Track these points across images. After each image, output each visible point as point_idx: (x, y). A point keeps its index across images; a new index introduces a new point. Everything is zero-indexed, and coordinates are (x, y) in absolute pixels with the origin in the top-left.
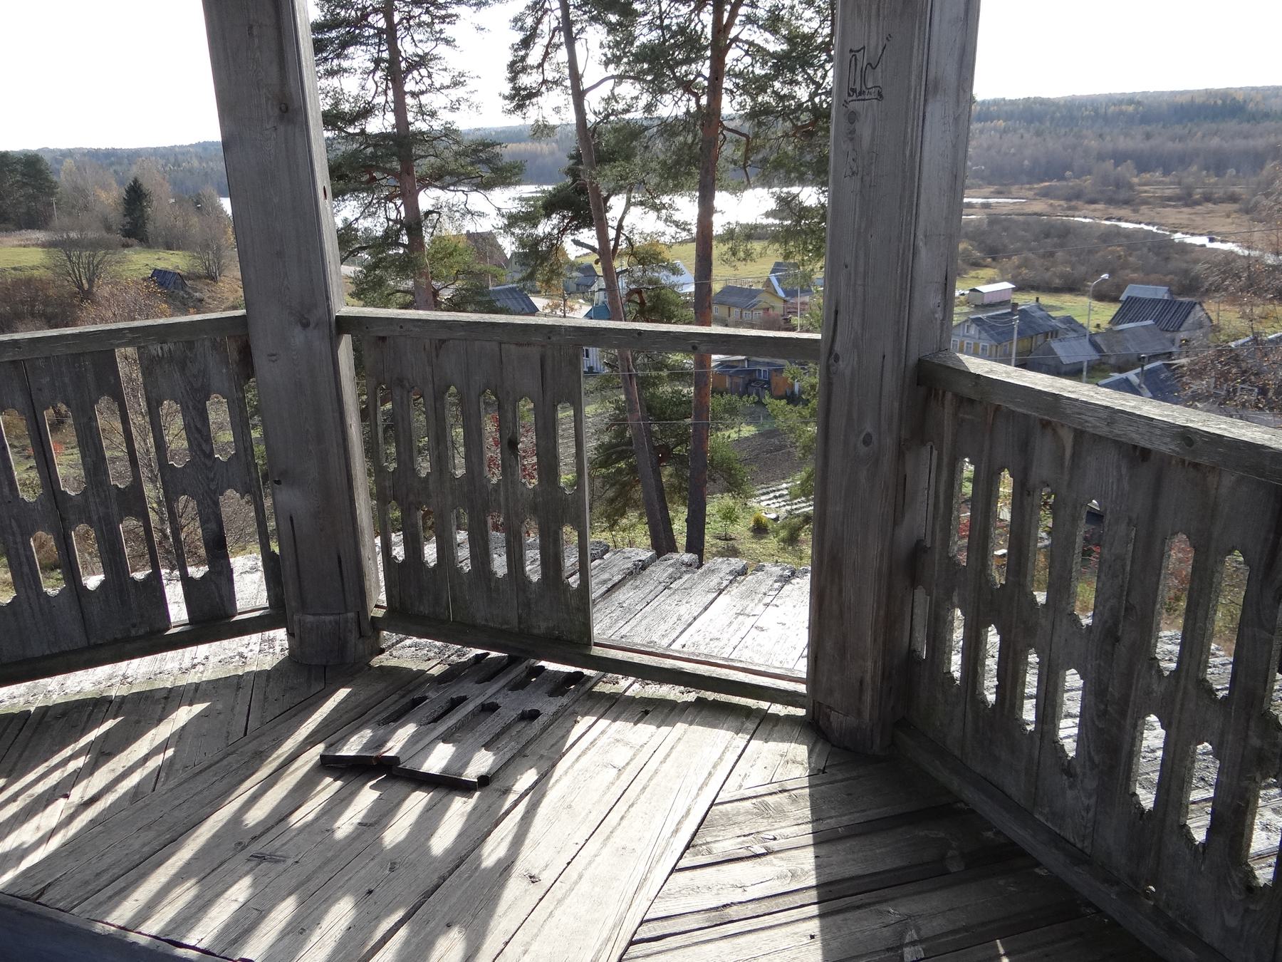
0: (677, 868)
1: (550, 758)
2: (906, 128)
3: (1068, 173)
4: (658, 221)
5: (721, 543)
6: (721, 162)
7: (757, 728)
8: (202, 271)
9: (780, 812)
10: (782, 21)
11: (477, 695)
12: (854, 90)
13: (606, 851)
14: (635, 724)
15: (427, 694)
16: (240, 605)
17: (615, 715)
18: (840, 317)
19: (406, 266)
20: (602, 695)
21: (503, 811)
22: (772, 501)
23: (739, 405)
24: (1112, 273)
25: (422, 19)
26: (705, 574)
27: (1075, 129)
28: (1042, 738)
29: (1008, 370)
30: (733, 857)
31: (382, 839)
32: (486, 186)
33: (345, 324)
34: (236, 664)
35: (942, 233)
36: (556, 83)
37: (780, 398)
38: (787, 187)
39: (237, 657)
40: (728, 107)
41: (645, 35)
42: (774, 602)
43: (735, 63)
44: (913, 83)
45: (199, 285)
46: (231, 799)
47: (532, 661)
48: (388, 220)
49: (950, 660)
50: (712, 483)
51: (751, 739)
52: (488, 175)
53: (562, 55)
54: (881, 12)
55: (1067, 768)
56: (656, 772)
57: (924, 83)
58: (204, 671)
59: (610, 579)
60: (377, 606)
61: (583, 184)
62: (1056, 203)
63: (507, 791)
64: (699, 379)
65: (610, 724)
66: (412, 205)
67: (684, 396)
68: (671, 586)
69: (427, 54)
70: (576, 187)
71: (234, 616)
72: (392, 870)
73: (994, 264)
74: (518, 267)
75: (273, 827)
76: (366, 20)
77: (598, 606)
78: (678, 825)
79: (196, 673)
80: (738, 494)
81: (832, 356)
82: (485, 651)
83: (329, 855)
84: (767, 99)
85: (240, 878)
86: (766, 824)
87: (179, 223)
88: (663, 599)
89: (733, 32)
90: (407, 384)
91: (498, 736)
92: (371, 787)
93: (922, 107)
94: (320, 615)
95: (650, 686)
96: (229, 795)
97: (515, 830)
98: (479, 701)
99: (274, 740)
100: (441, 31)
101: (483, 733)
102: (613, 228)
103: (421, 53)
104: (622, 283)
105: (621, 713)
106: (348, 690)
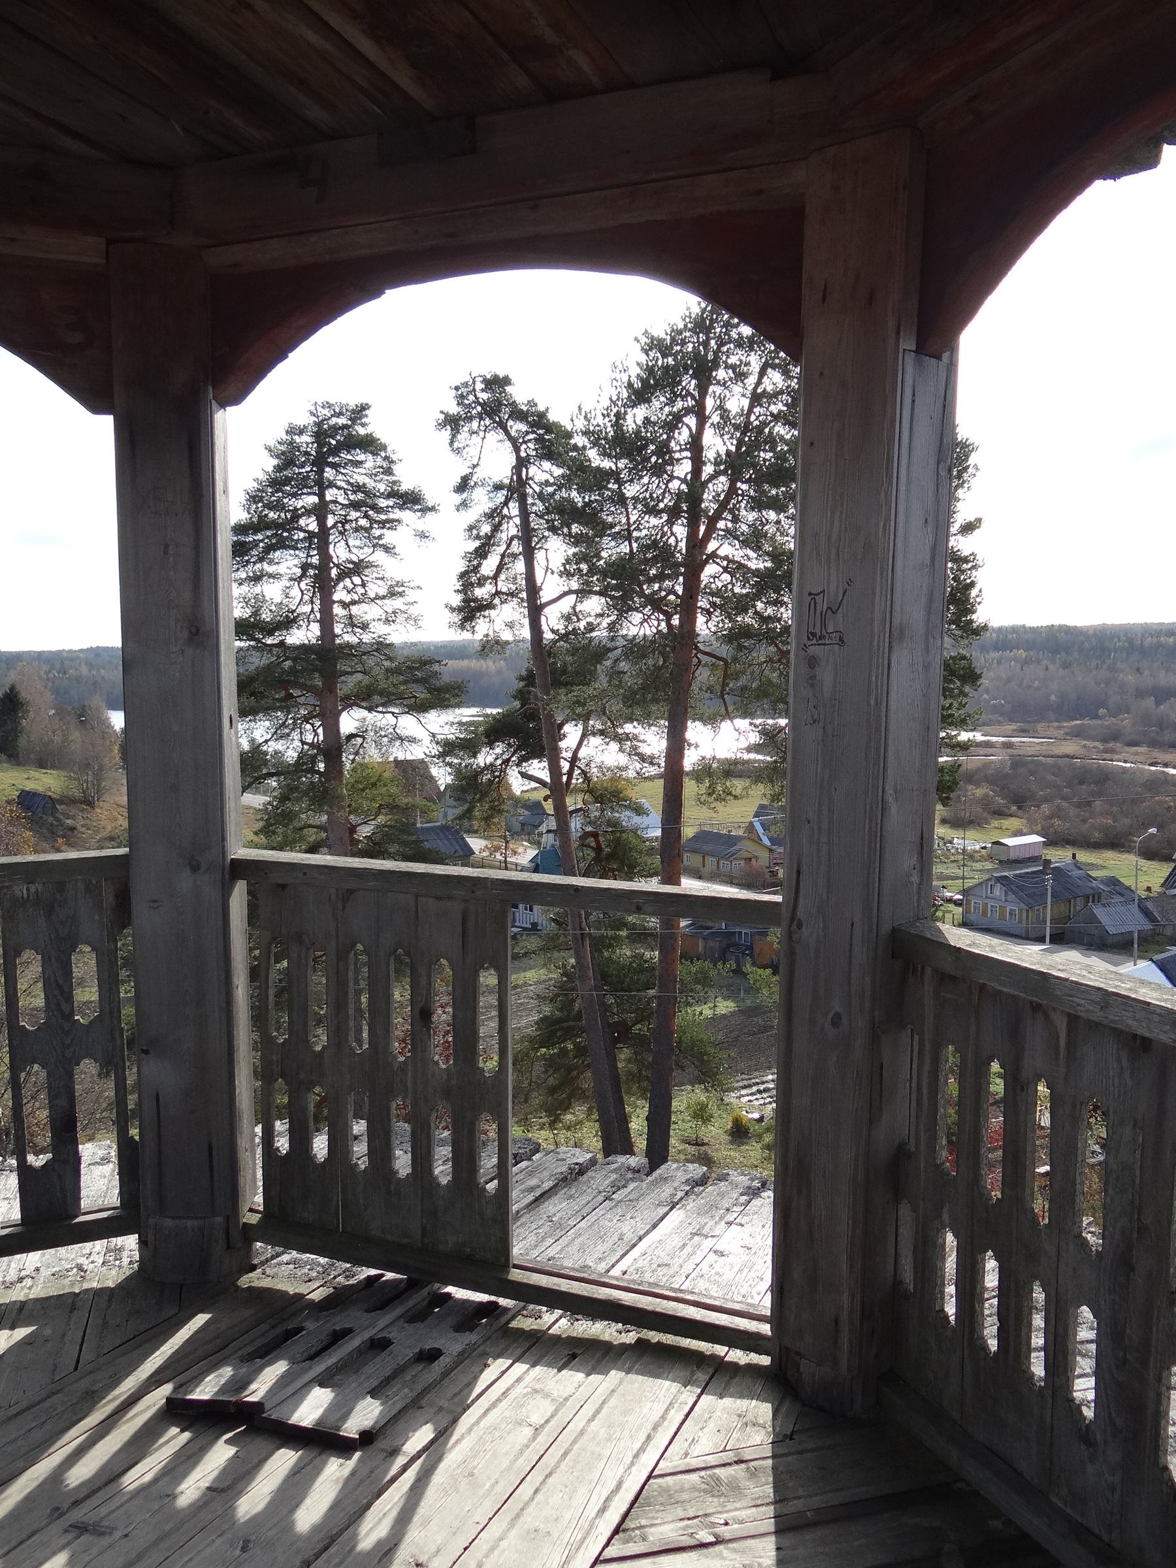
0: (601, 1558)
1: (451, 1412)
2: (870, 675)
3: (1102, 711)
4: (621, 754)
5: (691, 1149)
6: (695, 687)
7: (711, 1379)
8: (78, 794)
9: (735, 1489)
10: (766, 536)
11: (367, 1325)
12: (814, 635)
13: (513, 1532)
14: (559, 1370)
15: (303, 1324)
16: (84, 1204)
17: (534, 1359)
18: (803, 878)
19: (322, 796)
20: (520, 1332)
21: (388, 1477)
22: (755, 1097)
23: (713, 973)
24: (1160, 827)
25: (359, 523)
26: (655, 1183)
27: (1108, 662)
28: (1054, 1396)
29: (993, 943)
30: (672, 1546)
31: (235, 1509)
32: (420, 708)
33: (240, 869)
34: (73, 1278)
35: (915, 788)
36: (512, 594)
37: (764, 967)
38: (773, 718)
39: (75, 1270)
40: (703, 626)
41: (611, 550)
42: (737, 1220)
43: (712, 580)
44: (876, 630)
45: (73, 811)
46: (51, 1450)
47: (437, 1285)
48: (303, 743)
49: (942, 1293)
50: (680, 1071)
51: (702, 1393)
52: (423, 696)
53: (520, 566)
54: (841, 556)
55: (1084, 1434)
56: (582, 1432)
57: (888, 630)
58: (32, 1286)
59: (539, 1186)
60: (251, 1210)
61: (534, 709)
62: (1090, 744)
63: (394, 1452)
64: (666, 943)
65: (528, 1370)
66: (332, 727)
67: (646, 961)
68: (614, 1196)
69: (361, 561)
70: (525, 711)
71: (77, 1217)
72: (244, 1549)
73: (1020, 813)
74: (451, 802)
75: (99, 1489)
76: (297, 522)
77: (523, 1220)
78: (605, 1501)
79: (22, 1288)
80: (712, 1087)
81: (794, 923)
82: (380, 1272)
83: (168, 1527)
84: (748, 620)
85: (54, 1554)
86: (716, 1504)
87: (58, 739)
88: (602, 1212)
89: (712, 546)
90: (307, 941)
91: (387, 1382)
92: (226, 1442)
93: (886, 655)
94: (180, 1218)
95: (580, 1322)
96: (50, 1446)
97: (401, 1504)
98: (367, 1335)
99: (111, 1377)
100: (380, 537)
101: (370, 1376)
102: (565, 759)
103: (355, 559)
104: (576, 824)
105: (543, 1356)
106: (207, 1316)
